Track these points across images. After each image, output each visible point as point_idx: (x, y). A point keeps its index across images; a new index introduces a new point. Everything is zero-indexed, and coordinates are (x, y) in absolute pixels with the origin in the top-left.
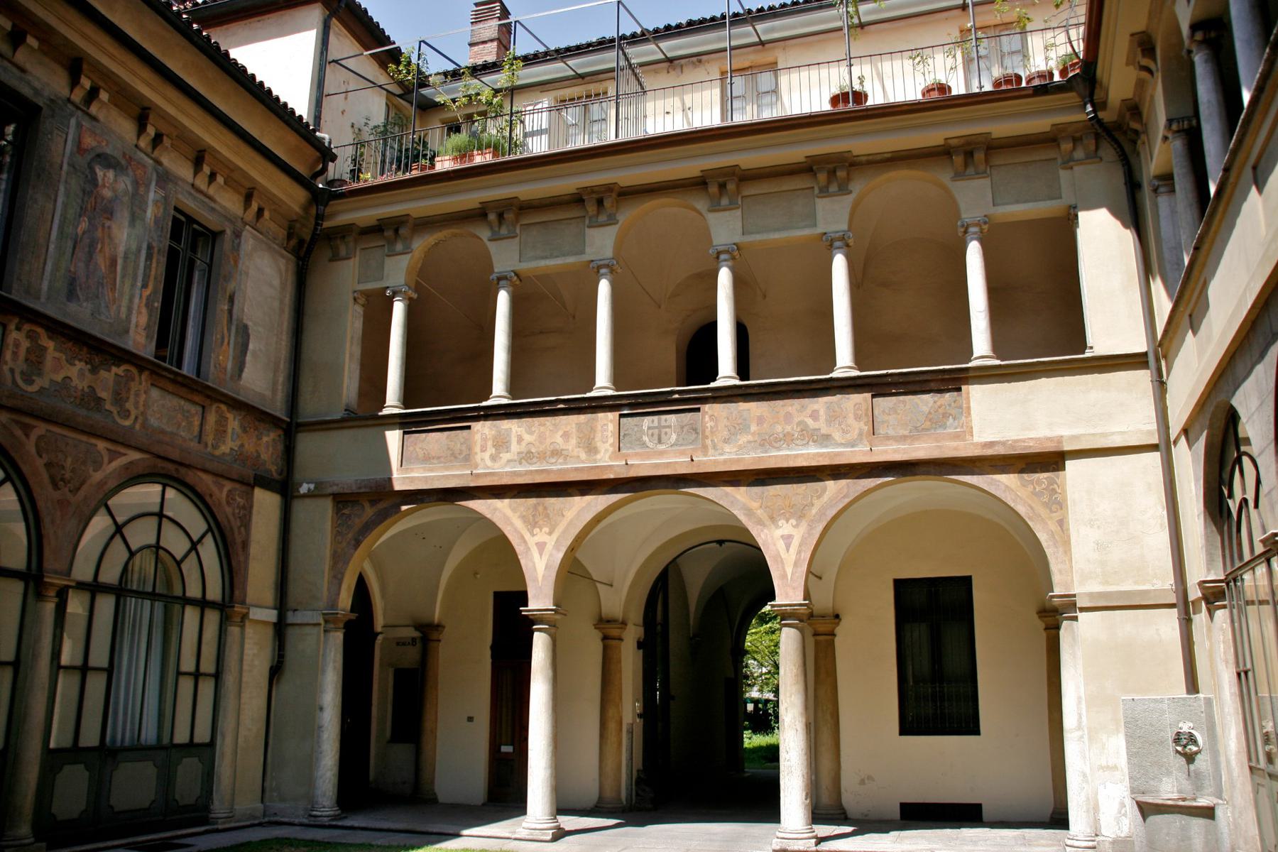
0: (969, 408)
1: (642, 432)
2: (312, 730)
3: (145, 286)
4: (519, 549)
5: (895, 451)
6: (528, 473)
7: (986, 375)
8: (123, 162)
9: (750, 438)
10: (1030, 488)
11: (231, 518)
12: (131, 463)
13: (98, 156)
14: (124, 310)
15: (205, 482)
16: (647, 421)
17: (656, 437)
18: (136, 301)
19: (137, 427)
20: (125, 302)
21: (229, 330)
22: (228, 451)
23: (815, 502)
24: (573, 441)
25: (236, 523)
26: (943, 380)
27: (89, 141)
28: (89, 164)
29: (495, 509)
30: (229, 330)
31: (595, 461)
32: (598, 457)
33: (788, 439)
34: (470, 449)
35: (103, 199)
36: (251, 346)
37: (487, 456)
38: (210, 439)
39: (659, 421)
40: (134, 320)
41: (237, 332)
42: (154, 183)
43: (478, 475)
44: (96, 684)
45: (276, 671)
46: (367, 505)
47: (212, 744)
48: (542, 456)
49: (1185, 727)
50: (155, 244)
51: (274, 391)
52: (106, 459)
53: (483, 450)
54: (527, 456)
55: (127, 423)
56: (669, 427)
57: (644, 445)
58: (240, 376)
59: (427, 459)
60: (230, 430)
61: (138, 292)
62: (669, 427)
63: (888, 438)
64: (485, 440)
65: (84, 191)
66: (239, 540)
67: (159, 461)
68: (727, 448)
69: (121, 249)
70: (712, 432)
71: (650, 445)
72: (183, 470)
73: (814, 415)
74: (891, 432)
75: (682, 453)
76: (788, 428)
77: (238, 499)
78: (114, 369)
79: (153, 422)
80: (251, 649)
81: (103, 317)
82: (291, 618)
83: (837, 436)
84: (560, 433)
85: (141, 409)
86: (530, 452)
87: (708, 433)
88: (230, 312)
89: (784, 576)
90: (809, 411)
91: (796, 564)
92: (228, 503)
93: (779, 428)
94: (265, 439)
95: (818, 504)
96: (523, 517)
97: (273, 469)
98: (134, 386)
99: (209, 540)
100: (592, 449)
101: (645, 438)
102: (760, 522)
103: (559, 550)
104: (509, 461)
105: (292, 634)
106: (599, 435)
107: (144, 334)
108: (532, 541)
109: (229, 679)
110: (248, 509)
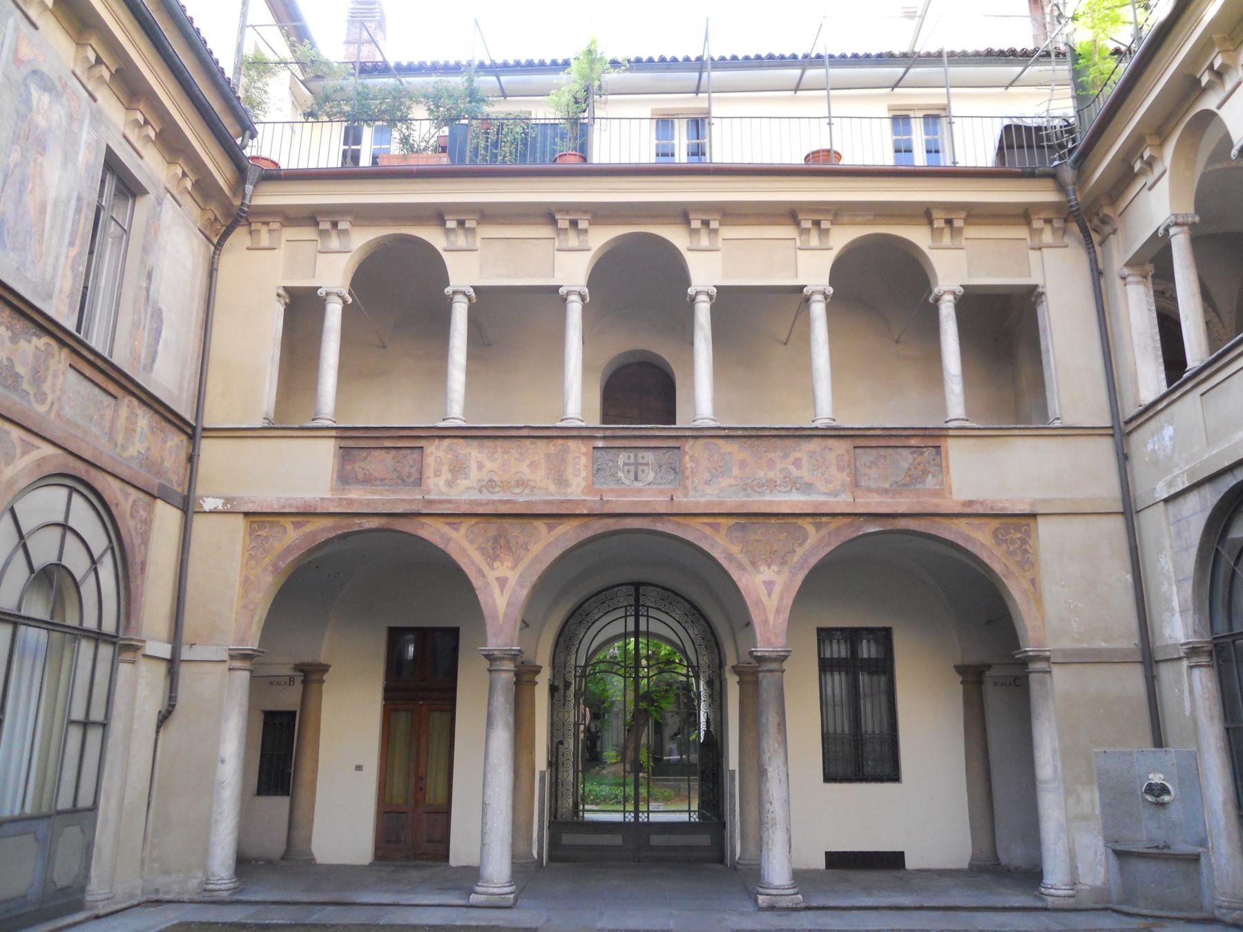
0: (948, 467)
1: (617, 467)
2: (208, 785)
3: (71, 244)
4: (476, 582)
5: (879, 504)
6: (489, 502)
7: (963, 433)
8: (59, 87)
9: (732, 481)
10: (1004, 546)
11: (134, 533)
12: (44, 458)
13: (35, 72)
14: (49, 269)
15: (111, 488)
16: (622, 457)
17: (632, 474)
18: (62, 260)
19: (52, 416)
20: (51, 261)
21: (146, 311)
22: (135, 454)
23: (797, 549)
24: (542, 473)
25: (137, 541)
26: (924, 436)
27: (26, 52)
28: (25, 79)
29: (449, 540)
30: (146, 311)
31: (566, 494)
32: (569, 490)
33: (772, 485)
34: (421, 473)
35: (37, 127)
36: (163, 334)
37: (441, 481)
38: (120, 438)
39: (636, 456)
40: (58, 284)
41: (152, 316)
42: (87, 122)
43: (431, 502)
44: (94, 736)
45: (164, 718)
46: (290, 527)
47: (94, 808)
48: (505, 486)
49: (1156, 778)
50: (85, 195)
51: (180, 388)
52: (19, 451)
53: (437, 474)
54: (491, 485)
55: (42, 409)
56: (647, 464)
57: (619, 481)
58: (152, 367)
59: (367, 481)
60: (139, 430)
61: (64, 250)
62: (647, 464)
63: (869, 490)
64: (439, 462)
65: (17, 112)
66: (139, 558)
67: (71, 459)
68: (708, 490)
69: (52, 194)
70: (692, 473)
71: (627, 482)
72: (93, 472)
73: (797, 463)
74: (872, 484)
75: (662, 492)
76: (771, 475)
77: (142, 512)
78: (35, 340)
79: (68, 412)
80: (143, 691)
81: (28, 274)
82: (186, 654)
83: (820, 485)
84: (527, 462)
85: (58, 393)
86: (491, 480)
87: (688, 473)
88: (148, 290)
89: (766, 621)
90: (791, 459)
91: (778, 611)
92: (132, 515)
93: (761, 474)
94: (170, 443)
95: (800, 552)
96: (482, 550)
97: (174, 478)
98: (52, 363)
99: (108, 560)
100: (561, 482)
101: (620, 474)
102: (740, 566)
103: (522, 587)
104: (467, 488)
105: (184, 671)
106: (569, 470)
107: (66, 301)
108: (492, 576)
109: (117, 726)
110: (148, 522)
